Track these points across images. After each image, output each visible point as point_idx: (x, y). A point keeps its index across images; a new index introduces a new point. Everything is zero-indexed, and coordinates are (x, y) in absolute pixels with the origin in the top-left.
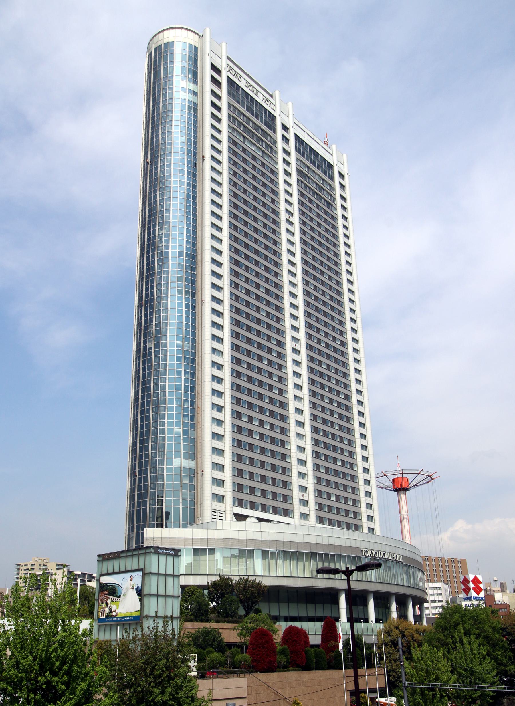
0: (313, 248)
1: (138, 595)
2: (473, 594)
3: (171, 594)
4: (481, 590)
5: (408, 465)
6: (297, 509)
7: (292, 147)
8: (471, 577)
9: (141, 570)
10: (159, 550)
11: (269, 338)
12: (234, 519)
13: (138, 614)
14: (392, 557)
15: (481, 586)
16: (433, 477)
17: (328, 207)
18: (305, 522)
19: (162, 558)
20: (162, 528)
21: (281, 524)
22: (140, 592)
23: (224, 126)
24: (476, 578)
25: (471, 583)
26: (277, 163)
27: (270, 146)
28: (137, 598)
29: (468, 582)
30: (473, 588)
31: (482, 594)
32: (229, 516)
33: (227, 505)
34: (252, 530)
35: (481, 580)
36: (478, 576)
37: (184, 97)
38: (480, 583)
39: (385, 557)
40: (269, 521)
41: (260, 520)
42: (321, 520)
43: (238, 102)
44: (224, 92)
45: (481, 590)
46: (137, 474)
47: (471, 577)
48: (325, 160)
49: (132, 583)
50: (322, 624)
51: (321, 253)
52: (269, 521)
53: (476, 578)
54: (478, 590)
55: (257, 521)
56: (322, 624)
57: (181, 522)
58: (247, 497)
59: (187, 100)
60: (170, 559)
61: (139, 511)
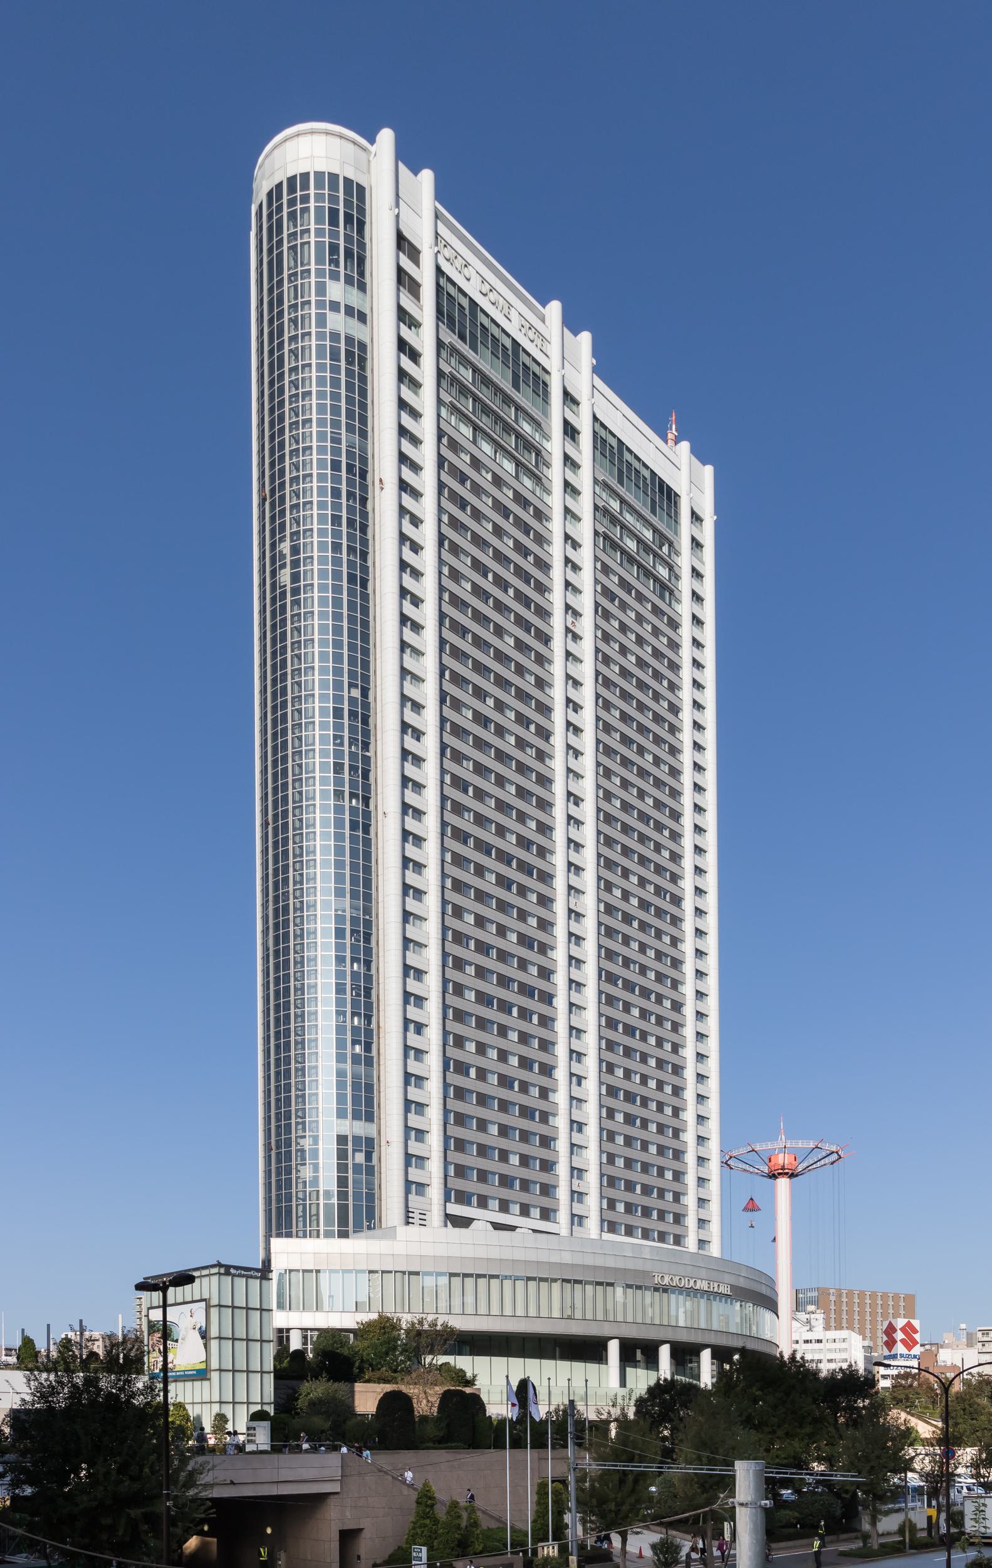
0: (625, 696)
1: (203, 1337)
2: (900, 1349)
4: (915, 1343)
7: (585, 452)
8: (900, 1323)
9: (205, 1300)
10: (232, 1271)
11: (523, 891)
13: (203, 1366)
15: (917, 1337)
17: (662, 597)
19: (241, 1282)
20: (318, 1236)
22: (204, 1335)
23: (426, 400)
24: (909, 1324)
25: (899, 1332)
26: (548, 492)
27: (529, 456)
28: (201, 1342)
29: (895, 1330)
30: (902, 1341)
31: (917, 1350)
34: (480, 1243)
35: (918, 1328)
36: (912, 1321)
38: (916, 1332)
39: (698, 1287)
40: (512, 1228)
41: (497, 1226)
43: (462, 337)
44: (426, 310)
45: (915, 1343)
46: (274, 1147)
47: (900, 1323)
48: (661, 482)
49: (193, 1320)
51: (641, 707)
52: (512, 1228)
53: (909, 1324)
54: (910, 1343)
58: (471, 1186)
60: (255, 1284)
61: (279, 1209)
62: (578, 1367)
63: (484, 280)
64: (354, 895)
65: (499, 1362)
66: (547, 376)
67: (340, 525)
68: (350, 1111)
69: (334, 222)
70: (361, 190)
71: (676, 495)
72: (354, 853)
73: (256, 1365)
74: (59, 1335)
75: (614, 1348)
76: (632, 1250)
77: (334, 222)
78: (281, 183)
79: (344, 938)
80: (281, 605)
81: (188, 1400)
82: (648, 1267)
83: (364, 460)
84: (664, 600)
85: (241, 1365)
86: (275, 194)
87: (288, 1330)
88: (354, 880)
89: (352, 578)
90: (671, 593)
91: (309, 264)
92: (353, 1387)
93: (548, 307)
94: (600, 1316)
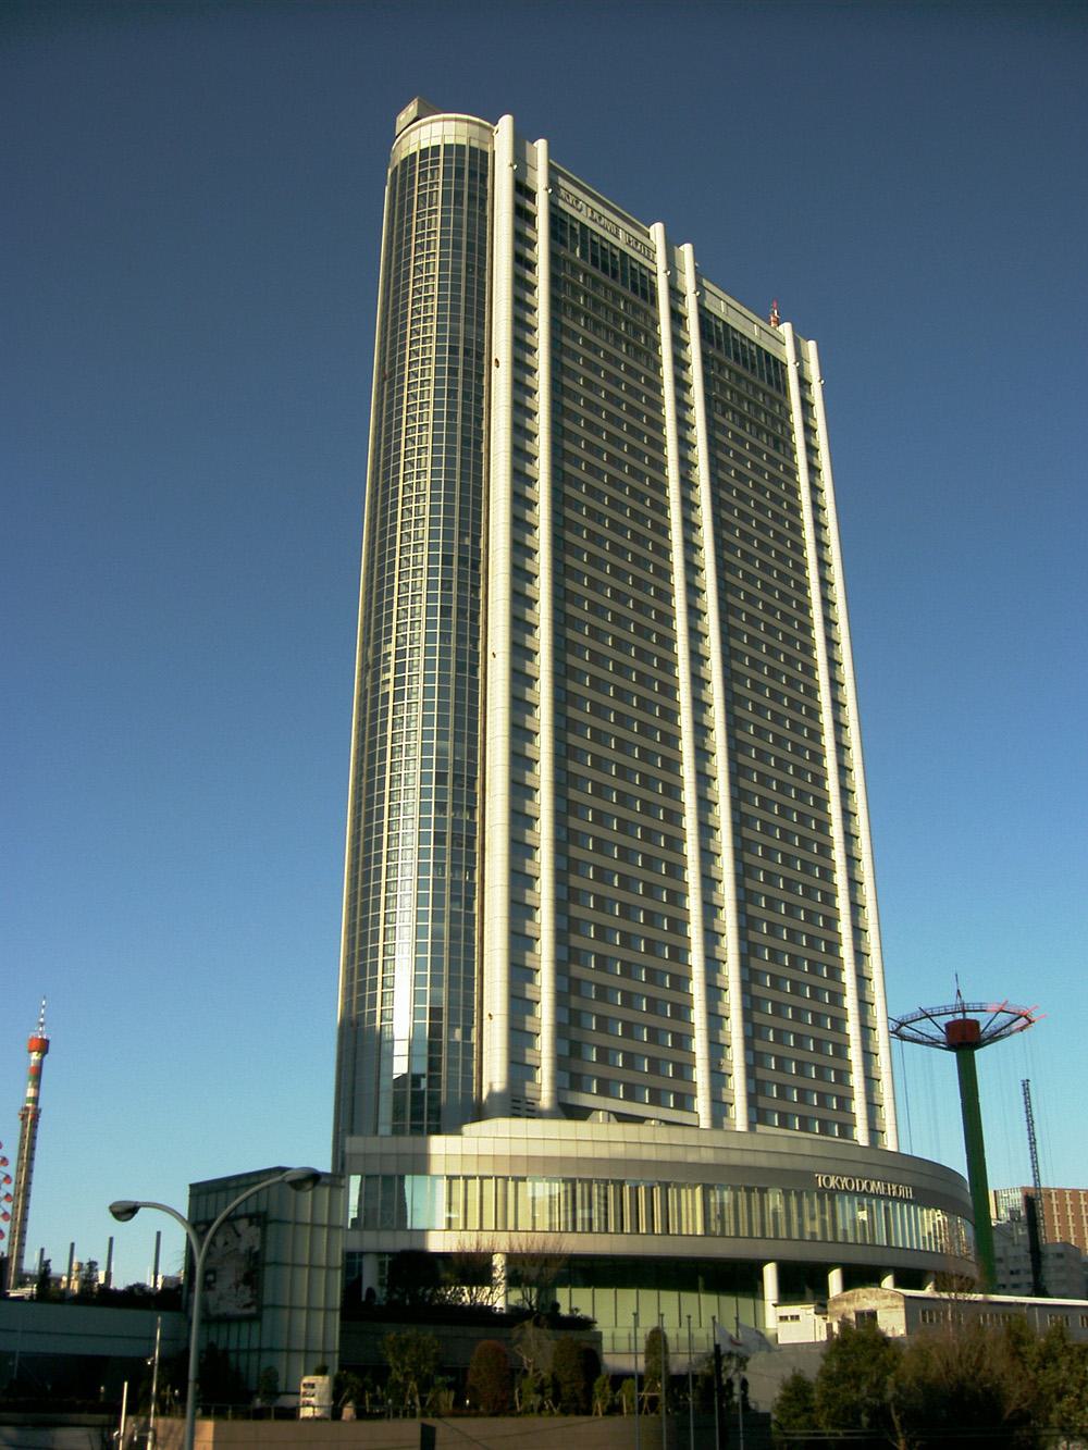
40: (640, 1120)
41: (623, 1118)
48: (768, 355)
62: (729, 1302)
63: (593, 210)
64: (458, 738)
65: (628, 1296)
66: (653, 277)
67: (456, 397)
68: (451, 732)
69: (458, 201)
70: (484, 154)
71: (783, 364)
72: (459, 694)
73: (320, 1301)
74: (82, 1257)
75: (770, 1273)
76: (782, 1143)
77: (458, 201)
78: (415, 153)
79: (448, 697)
80: (391, 377)
81: (233, 1345)
82: (806, 1165)
83: (480, 345)
84: (779, 451)
85: (320, 1301)
86: (404, 162)
87: (362, 1254)
88: (458, 722)
89: (465, 441)
90: (785, 445)
91: (436, 204)
92: (426, 1145)
93: (652, 227)
94: (757, 1233)
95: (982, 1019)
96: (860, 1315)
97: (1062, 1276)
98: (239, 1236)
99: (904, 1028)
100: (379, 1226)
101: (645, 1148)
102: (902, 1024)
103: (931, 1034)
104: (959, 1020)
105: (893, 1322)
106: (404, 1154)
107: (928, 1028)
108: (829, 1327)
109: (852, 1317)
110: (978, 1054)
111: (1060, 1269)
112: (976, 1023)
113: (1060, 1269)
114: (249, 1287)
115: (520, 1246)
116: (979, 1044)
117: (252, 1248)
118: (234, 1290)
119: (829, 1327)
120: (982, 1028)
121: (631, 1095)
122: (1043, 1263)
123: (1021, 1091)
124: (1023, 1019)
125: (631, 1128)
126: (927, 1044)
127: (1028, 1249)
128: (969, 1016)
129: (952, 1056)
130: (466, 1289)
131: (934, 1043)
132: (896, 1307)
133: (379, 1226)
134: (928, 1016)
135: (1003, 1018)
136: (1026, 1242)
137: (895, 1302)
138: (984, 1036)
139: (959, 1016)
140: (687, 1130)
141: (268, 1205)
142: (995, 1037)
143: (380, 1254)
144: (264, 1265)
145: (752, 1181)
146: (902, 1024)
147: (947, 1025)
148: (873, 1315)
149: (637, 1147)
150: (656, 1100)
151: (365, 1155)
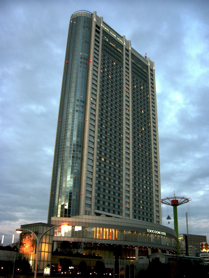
3: (49, 253)
5: (174, 194)
6: (124, 211)
12: (95, 215)
14: (161, 233)
16: (189, 200)
18: (128, 218)
21: (117, 219)
32: (93, 213)
33: (92, 209)
37: (82, 105)
40: (111, 216)
41: (107, 216)
42: (135, 217)
50: (174, 229)
52: (111, 216)
55: (105, 216)
56: (174, 229)
57: (64, 215)
59: (79, 100)
95: (179, 200)
96: (156, 258)
97: (191, 252)
98: (31, 236)
99: (163, 201)
100: (74, 237)
101: (119, 223)
102: (163, 200)
103: (169, 202)
104: (174, 200)
105: (163, 260)
106: (53, 221)
107: (167, 201)
108: (149, 260)
109: (154, 258)
110: (178, 207)
111: (191, 250)
112: (177, 201)
113: (191, 250)
114: (33, 247)
115: (88, 241)
116: (178, 205)
117: (34, 239)
118: (29, 248)
119: (149, 260)
120: (179, 202)
121: (109, 211)
122: (188, 249)
123: (185, 215)
124: (187, 200)
125: (110, 218)
126: (167, 204)
127: (185, 246)
128: (176, 199)
129: (172, 207)
130: (76, 249)
131: (169, 204)
132: (163, 257)
133: (74, 237)
134: (168, 199)
135: (183, 200)
136: (185, 245)
137: (163, 256)
138: (179, 203)
139: (174, 199)
140: (119, 219)
141: (38, 230)
142: (181, 204)
143: (57, 241)
144: (105, 251)
145: (133, 229)
146: (163, 200)
147: (172, 201)
148: (158, 259)
149: (111, 222)
150: (114, 212)
151: (55, 221)
